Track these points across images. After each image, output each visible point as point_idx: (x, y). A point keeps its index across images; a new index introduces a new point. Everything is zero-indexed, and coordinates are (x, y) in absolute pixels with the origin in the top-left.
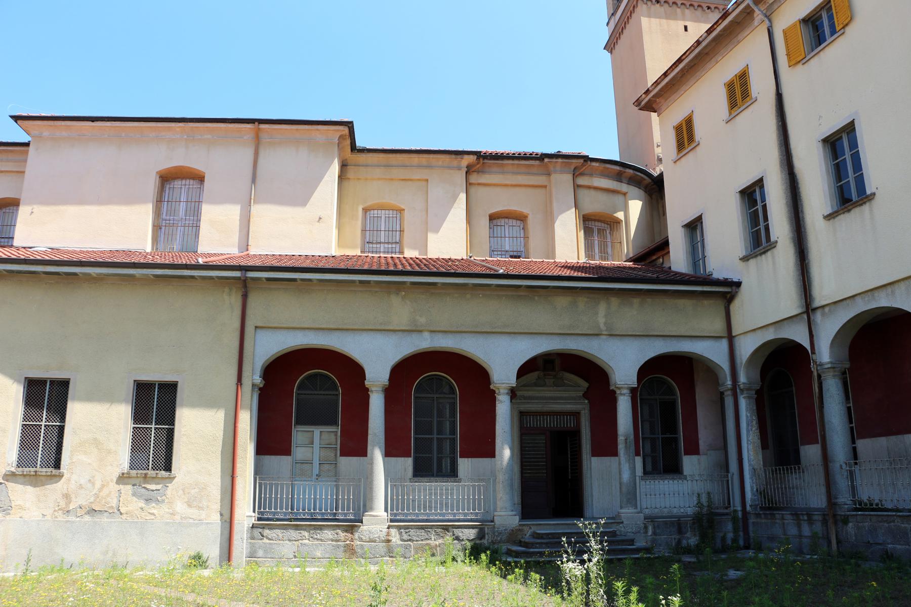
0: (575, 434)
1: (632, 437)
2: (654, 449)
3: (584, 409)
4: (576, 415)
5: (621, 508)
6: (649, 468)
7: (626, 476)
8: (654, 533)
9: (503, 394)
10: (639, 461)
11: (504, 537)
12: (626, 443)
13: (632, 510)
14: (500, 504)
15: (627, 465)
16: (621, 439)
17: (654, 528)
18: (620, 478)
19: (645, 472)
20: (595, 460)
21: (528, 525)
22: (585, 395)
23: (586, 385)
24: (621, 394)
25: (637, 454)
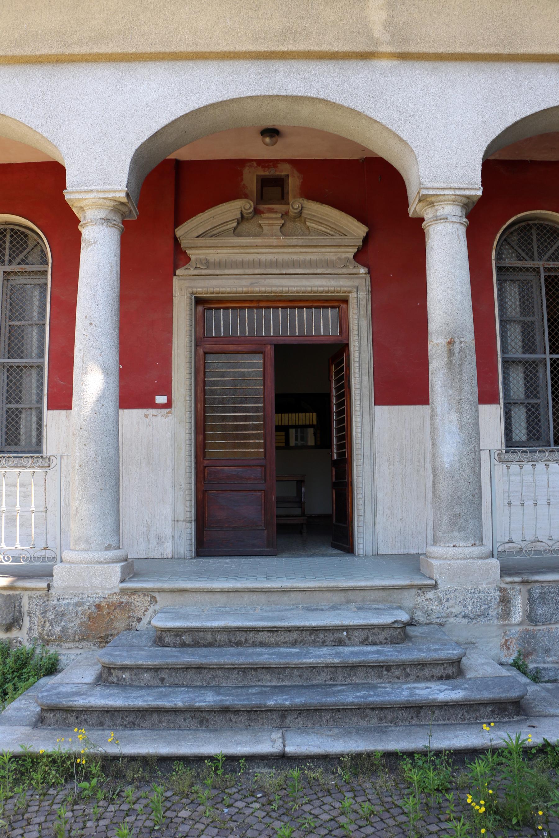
0: (337, 354)
1: (469, 337)
2: (531, 389)
3: (356, 286)
4: (339, 303)
5: (435, 541)
6: (520, 432)
7: (450, 449)
8: (531, 618)
9: (94, 222)
10: (492, 416)
11: (73, 626)
12: (451, 352)
13: (465, 549)
14: (75, 529)
15: (454, 417)
16: (436, 342)
17: (531, 600)
18: (434, 456)
19: (510, 442)
20: (384, 412)
21: (145, 592)
22: (360, 257)
23: (361, 230)
24: (437, 219)
25: (487, 396)
